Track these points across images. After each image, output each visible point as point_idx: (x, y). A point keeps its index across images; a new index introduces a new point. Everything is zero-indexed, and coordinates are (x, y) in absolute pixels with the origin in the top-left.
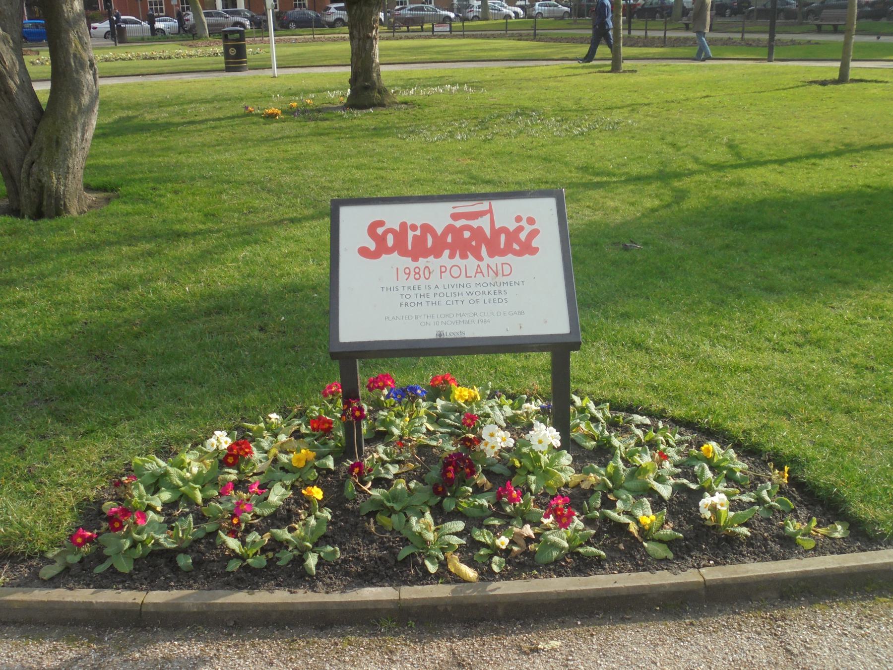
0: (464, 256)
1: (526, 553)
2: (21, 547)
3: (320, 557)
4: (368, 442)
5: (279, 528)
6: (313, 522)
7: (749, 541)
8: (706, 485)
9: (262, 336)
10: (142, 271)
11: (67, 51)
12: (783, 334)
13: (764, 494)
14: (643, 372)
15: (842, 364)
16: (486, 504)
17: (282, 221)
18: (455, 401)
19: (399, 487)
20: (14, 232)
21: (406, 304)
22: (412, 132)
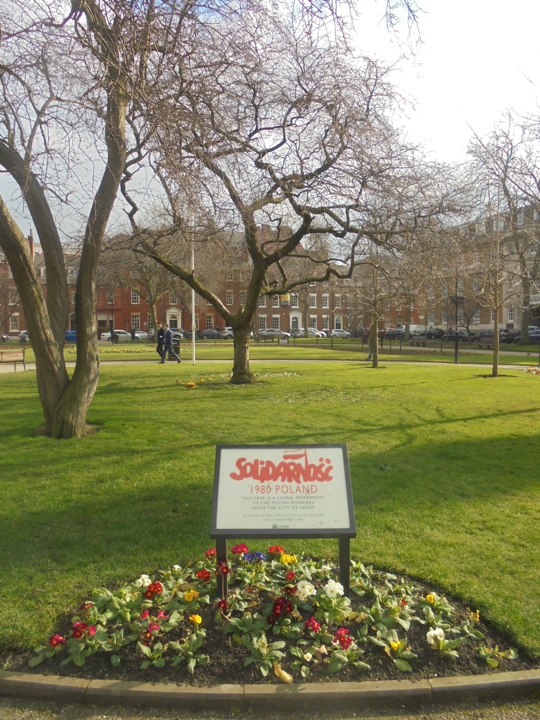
0: (290, 480)
1: (323, 664)
2: (20, 644)
3: (197, 662)
4: (231, 586)
5: (174, 641)
6: (194, 637)
7: (458, 661)
8: (431, 621)
9: (175, 515)
10: (111, 472)
12: (471, 523)
13: (465, 628)
14: (392, 545)
15: (506, 542)
16: (299, 630)
17: (191, 446)
18: (283, 563)
19: (247, 617)
20: (46, 446)
21: (256, 508)
22: (265, 398)
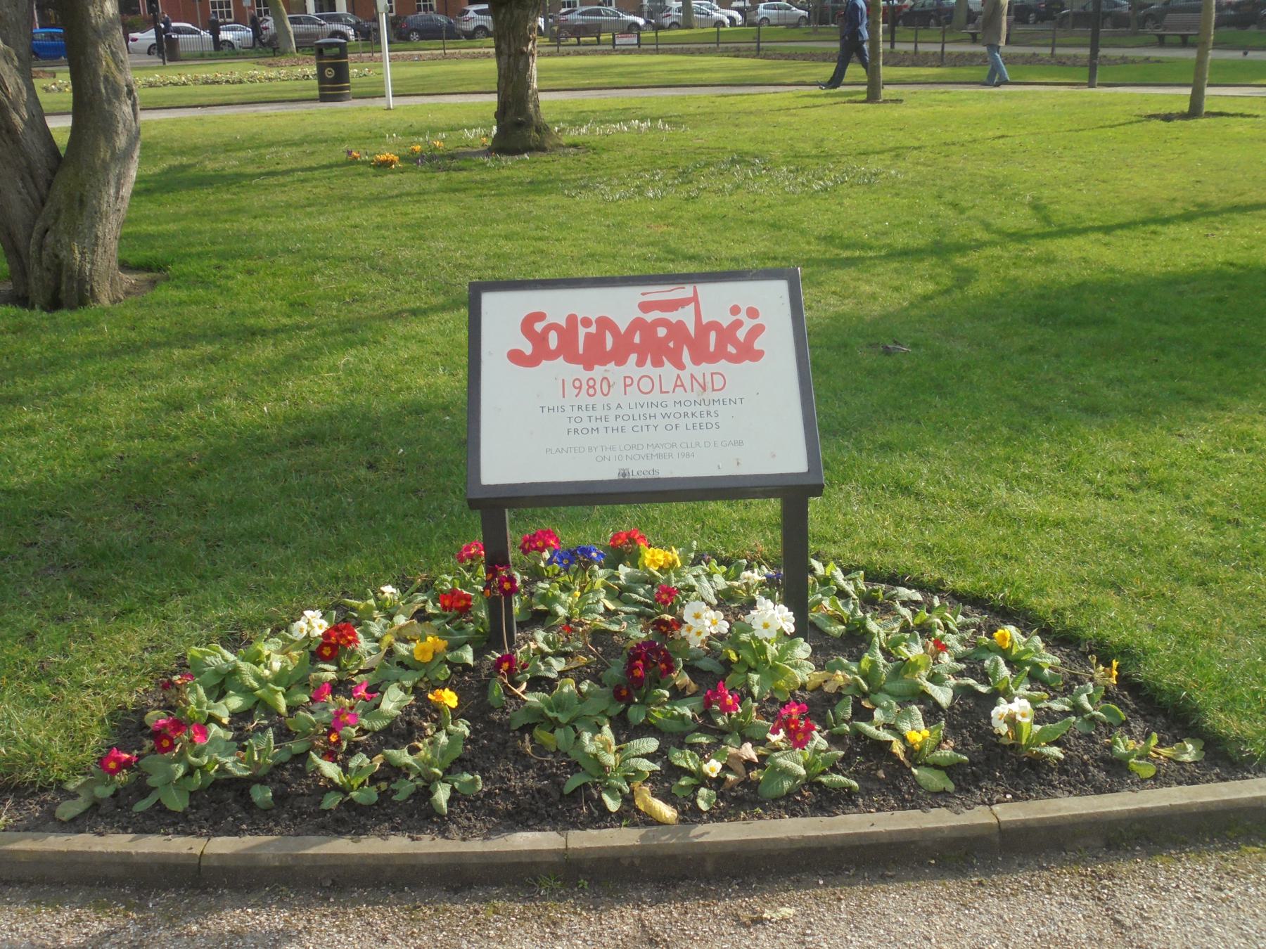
0: (657, 363)
1: (746, 783)
2: (30, 775)
3: (453, 790)
4: (522, 626)
5: (395, 747)
6: (443, 739)
7: (1062, 767)
8: (1001, 687)
9: (372, 475)
10: (201, 383)
12: (1111, 473)
13: (1084, 699)
14: (911, 527)
15: (1194, 515)
16: (689, 713)
17: (399, 313)
18: (645, 568)
19: (566, 690)
20: (19, 329)
21: (576, 431)
22: (585, 187)
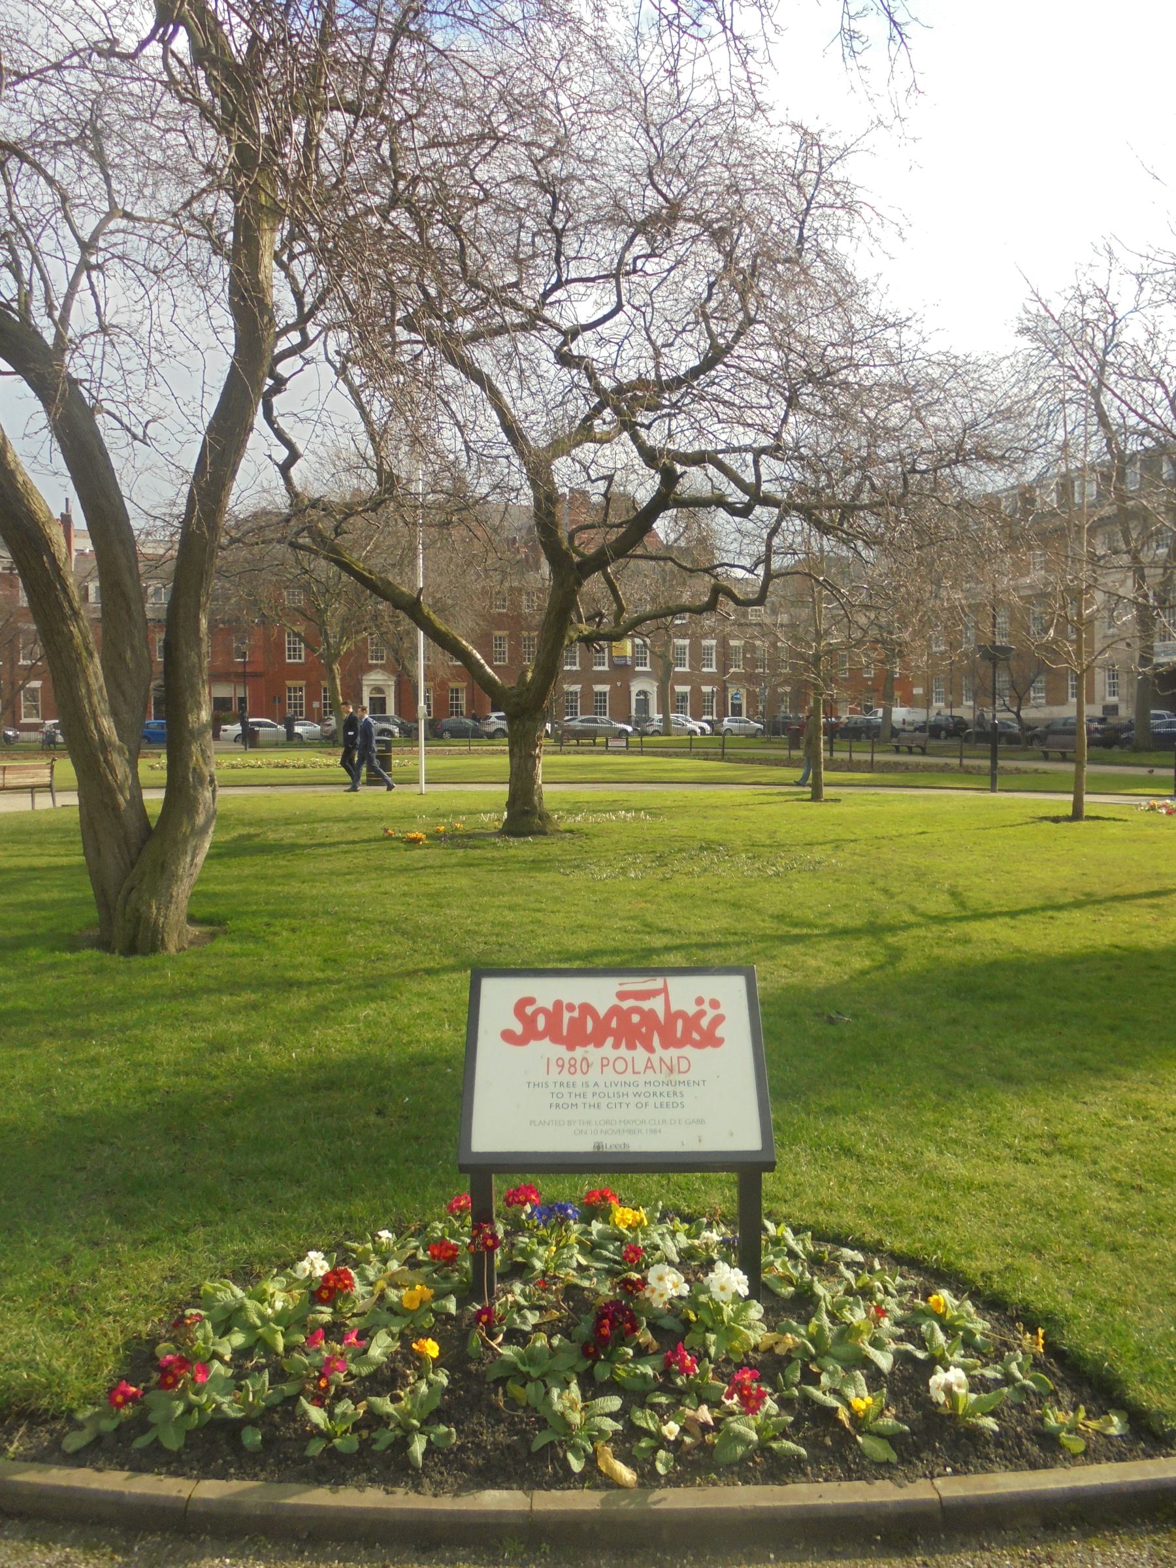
0: (631, 1046)
1: (702, 1446)
2: (44, 1402)
3: (429, 1442)
4: (503, 1277)
5: (379, 1395)
6: (423, 1388)
7: (998, 1439)
8: (938, 1353)
9: (380, 1121)
10: (242, 1028)
11: (187, 767)
12: (1027, 1139)
13: (1014, 1367)
14: (853, 1188)
15: (1102, 1181)
16: (650, 1372)
17: (416, 972)
18: (616, 1226)
19: (538, 1344)
20: (99, 971)
21: (557, 1106)
22: (578, 866)
